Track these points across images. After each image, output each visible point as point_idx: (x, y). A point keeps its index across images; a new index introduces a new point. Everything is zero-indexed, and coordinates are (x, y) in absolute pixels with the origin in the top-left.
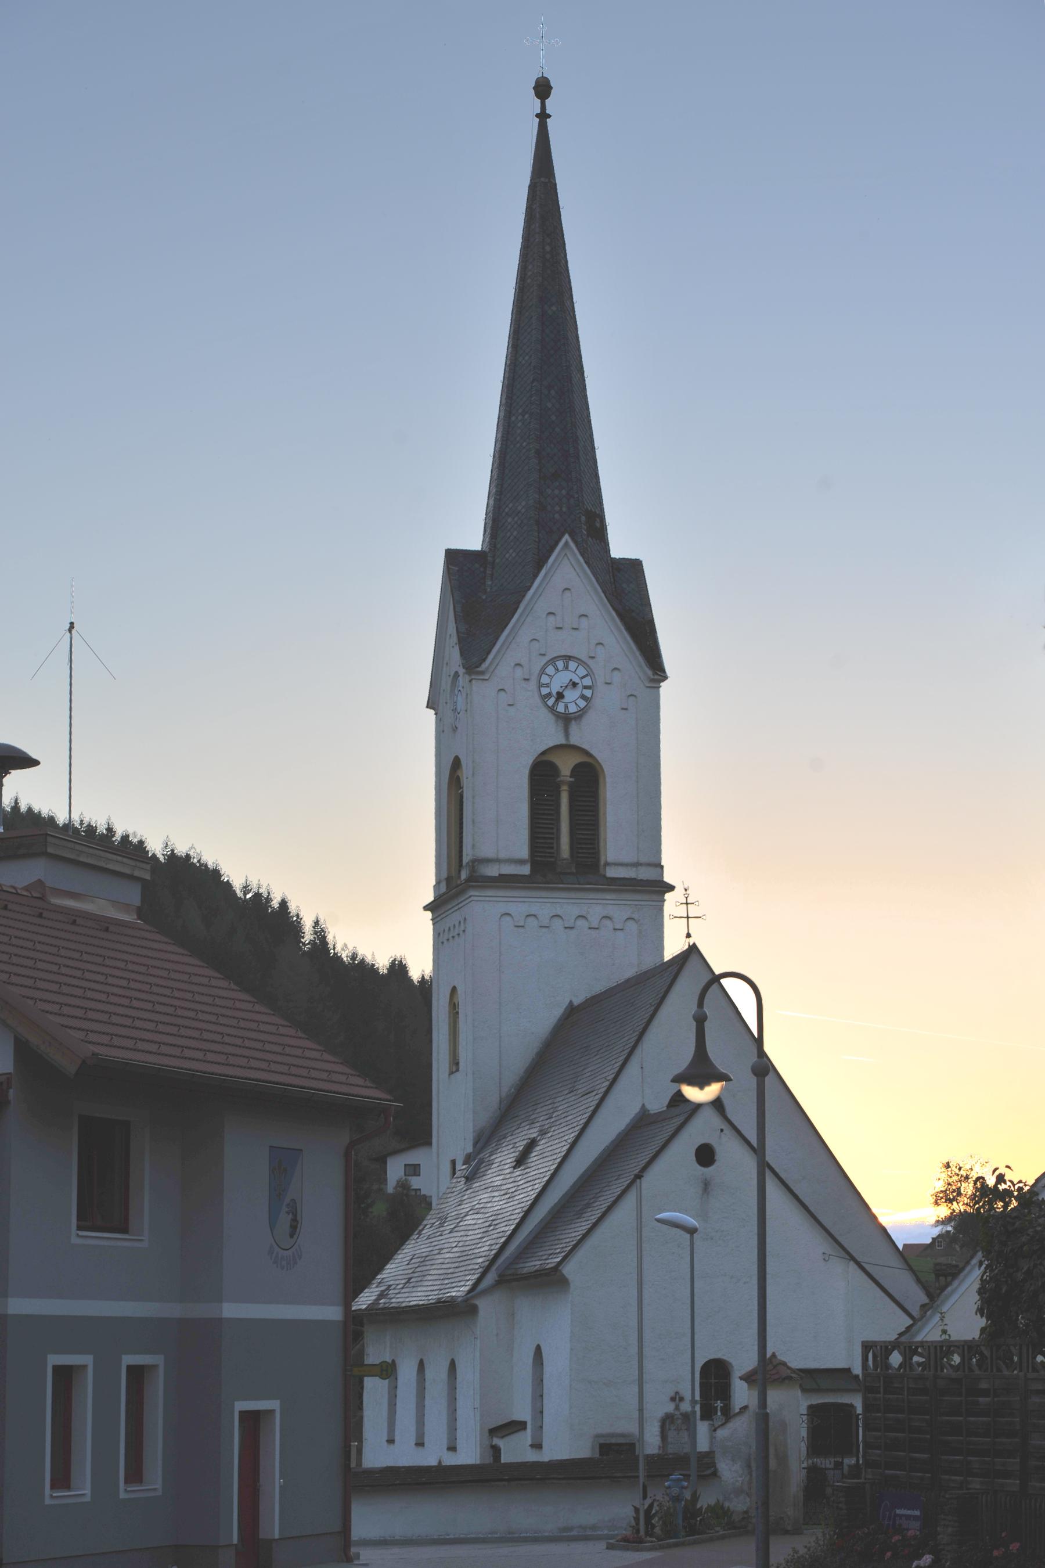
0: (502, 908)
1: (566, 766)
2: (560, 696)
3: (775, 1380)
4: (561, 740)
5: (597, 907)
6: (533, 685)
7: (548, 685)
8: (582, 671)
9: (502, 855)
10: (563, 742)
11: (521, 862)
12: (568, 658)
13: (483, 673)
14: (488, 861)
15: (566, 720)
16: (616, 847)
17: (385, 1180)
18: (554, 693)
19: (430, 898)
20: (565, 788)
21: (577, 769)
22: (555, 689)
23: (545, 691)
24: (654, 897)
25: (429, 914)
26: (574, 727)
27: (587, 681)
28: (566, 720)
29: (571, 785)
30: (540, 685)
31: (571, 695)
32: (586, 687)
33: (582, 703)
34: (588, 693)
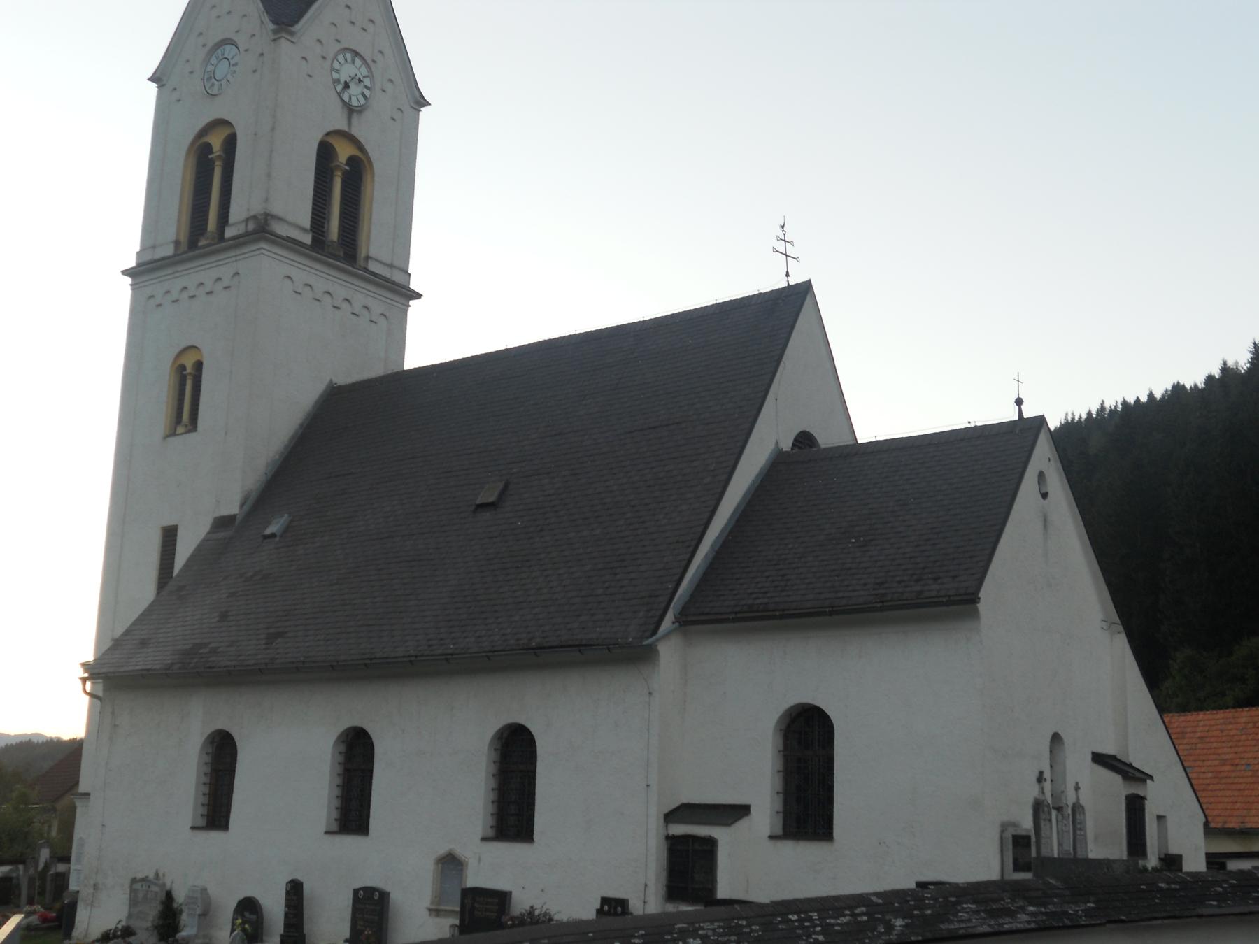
0: (294, 272)
1: (344, 152)
2: (347, 86)
3: (962, 440)
4: (342, 126)
5: (362, 295)
6: (327, 64)
7: (338, 71)
8: (364, 71)
9: (289, 218)
10: (345, 128)
11: (304, 230)
12: (356, 54)
13: (292, 34)
14: (280, 219)
15: (351, 110)
16: (374, 243)
17: (172, 568)
18: (342, 81)
19: (132, 263)
20: (339, 173)
21: (352, 160)
22: (344, 77)
23: (336, 76)
24: (402, 300)
25: (128, 280)
26: (355, 118)
27: (367, 82)
28: (351, 110)
29: (345, 173)
30: (333, 69)
31: (355, 90)
32: (366, 87)
33: (363, 101)
34: (367, 93)
